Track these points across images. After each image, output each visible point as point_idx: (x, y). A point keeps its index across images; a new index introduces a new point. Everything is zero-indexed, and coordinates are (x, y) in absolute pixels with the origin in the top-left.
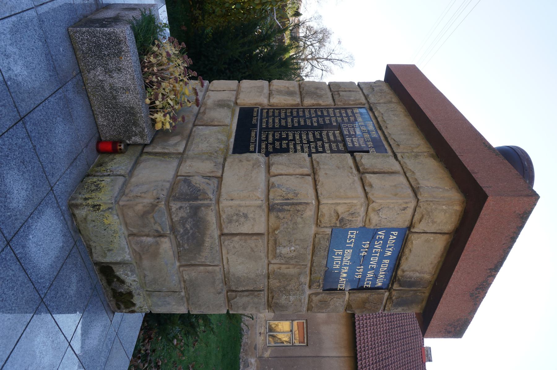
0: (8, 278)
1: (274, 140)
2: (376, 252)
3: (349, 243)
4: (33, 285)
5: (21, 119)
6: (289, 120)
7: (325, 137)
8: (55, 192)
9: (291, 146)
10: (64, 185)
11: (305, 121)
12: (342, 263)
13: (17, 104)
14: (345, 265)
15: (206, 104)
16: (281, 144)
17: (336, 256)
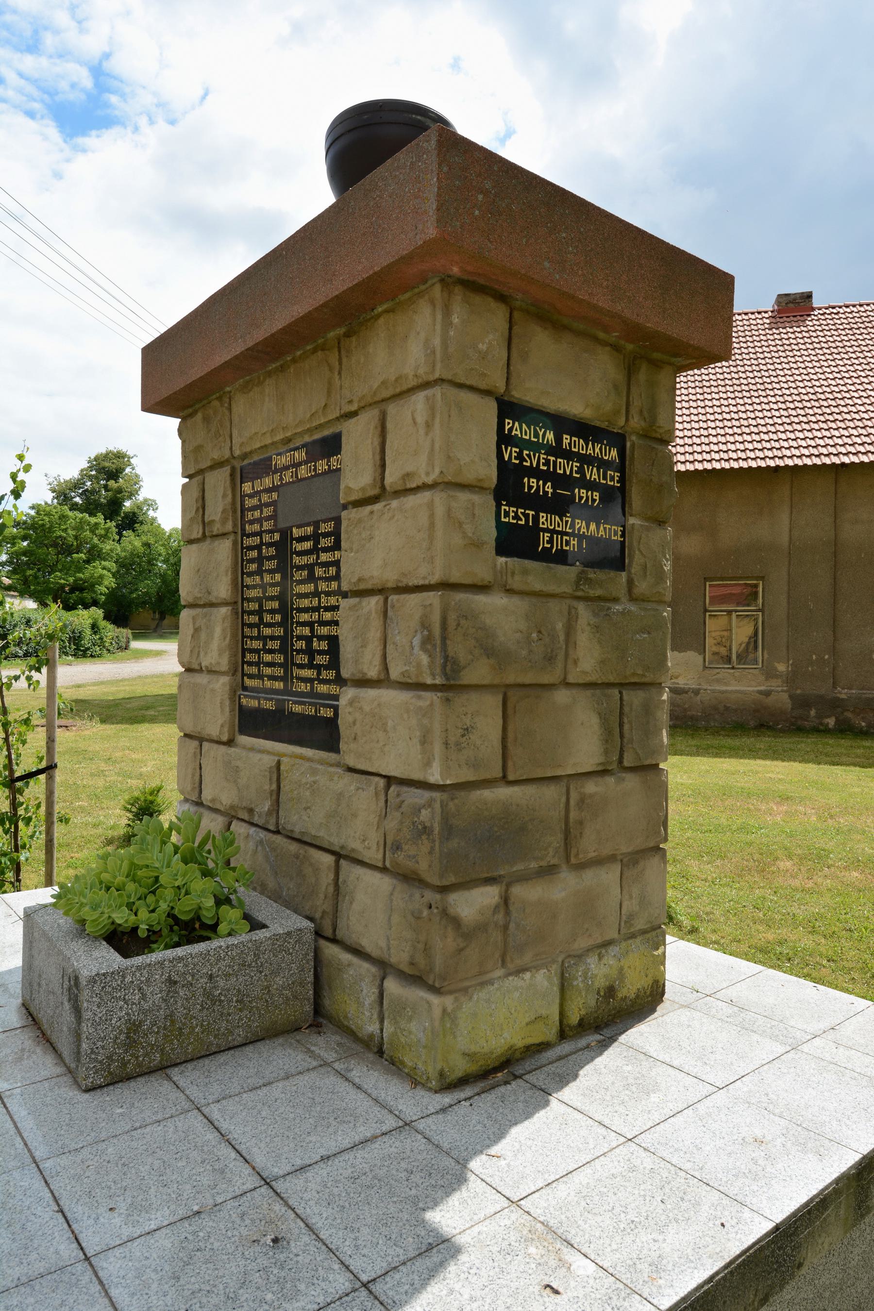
0: (583, 1204)
1: (311, 666)
2: (547, 463)
3: (527, 520)
4: (598, 1157)
5: (268, 1184)
6: (267, 631)
7: (305, 558)
8: (414, 1118)
9: (324, 631)
10: (401, 1101)
11: (272, 598)
12: (567, 534)
13: (238, 1192)
14: (573, 526)
15: (232, 807)
16: (320, 652)
17: (552, 547)
